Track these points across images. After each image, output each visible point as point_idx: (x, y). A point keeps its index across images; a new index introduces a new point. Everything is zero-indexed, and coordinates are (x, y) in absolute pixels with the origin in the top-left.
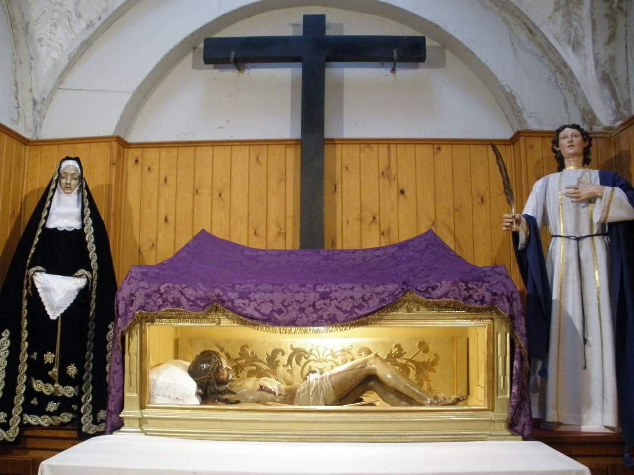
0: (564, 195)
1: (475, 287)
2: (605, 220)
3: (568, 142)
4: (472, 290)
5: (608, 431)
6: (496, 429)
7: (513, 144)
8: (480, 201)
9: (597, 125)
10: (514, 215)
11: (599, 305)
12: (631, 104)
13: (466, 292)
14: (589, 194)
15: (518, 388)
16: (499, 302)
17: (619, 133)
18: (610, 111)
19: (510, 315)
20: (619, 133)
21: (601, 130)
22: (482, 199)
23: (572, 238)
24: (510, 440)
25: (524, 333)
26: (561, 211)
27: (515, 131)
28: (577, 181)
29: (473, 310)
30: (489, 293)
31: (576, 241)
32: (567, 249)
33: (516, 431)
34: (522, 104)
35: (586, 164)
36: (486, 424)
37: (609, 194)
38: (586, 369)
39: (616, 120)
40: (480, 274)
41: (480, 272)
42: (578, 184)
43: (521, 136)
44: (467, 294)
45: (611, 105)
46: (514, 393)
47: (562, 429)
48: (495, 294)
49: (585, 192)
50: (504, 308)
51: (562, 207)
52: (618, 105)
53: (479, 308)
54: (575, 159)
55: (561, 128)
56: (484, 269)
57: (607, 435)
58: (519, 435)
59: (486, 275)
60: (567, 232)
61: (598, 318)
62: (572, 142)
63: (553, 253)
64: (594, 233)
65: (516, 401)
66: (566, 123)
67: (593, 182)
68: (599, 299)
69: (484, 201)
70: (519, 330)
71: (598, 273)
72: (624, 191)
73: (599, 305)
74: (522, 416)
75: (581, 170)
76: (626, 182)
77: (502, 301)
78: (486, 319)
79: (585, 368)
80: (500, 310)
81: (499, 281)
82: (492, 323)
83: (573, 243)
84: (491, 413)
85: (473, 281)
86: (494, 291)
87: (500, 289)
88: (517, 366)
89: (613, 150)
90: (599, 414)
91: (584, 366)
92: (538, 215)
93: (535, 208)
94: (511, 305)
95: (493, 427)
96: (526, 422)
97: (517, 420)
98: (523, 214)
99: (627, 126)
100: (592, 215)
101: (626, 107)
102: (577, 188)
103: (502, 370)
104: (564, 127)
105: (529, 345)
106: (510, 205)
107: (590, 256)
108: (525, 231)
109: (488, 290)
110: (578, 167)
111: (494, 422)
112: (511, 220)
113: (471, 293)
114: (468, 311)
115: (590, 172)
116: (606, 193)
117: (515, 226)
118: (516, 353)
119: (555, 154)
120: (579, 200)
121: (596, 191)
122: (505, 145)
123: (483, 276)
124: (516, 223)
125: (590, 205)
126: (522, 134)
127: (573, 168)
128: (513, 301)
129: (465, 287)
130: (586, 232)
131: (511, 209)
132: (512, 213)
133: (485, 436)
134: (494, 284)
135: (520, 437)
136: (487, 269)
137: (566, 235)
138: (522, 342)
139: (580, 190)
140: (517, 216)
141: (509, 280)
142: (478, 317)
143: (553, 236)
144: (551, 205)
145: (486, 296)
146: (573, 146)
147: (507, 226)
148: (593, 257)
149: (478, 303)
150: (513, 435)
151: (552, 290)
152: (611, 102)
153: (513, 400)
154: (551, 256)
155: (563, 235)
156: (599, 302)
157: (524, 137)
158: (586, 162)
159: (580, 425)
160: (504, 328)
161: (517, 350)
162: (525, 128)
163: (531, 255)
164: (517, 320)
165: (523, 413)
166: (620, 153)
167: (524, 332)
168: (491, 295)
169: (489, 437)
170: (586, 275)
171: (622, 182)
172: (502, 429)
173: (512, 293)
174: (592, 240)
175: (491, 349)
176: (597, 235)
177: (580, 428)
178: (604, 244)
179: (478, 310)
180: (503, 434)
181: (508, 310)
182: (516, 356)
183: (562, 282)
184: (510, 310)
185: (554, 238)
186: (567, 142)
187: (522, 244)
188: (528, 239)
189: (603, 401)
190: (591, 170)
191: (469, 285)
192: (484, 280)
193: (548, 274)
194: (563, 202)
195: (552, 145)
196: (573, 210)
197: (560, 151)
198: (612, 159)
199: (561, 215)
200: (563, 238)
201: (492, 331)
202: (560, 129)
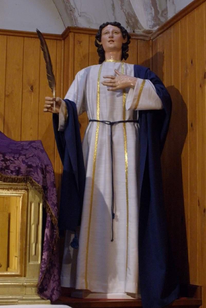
0: (102, 83)
1: (12, 159)
2: (135, 108)
3: (109, 37)
4: (9, 162)
5: (130, 298)
6: (27, 294)
7: (64, 39)
8: (30, 89)
9: (139, 28)
10: (54, 97)
11: (127, 184)
12: (167, 13)
13: (3, 163)
14: (123, 84)
15: (48, 254)
16: (33, 173)
17: (156, 37)
18: (150, 17)
19: (42, 186)
20: (156, 37)
21: (142, 33)
22: (32, 88)
23: (106, 122)
24: (39, 303)
25: (55, 203)
26: (98, 98)
27: (66, 27)
28: (114, 72)
29: (8, 180)
30: (24, 165)
31: (110, 126)
32: (102, 131)
33: (46, 296)
34: (75, 4)
35: (124, 59)
36: (18, 289)
37: (140, 85)
38: (113, 241)
39: (154, 26)
40: (18, 147)
41: (18, 145)
42: (115, 75)
43: (70, 32)
44: (5, 165)
45: (151, 12)
46: (44, 259)
47: (90, 296)
48: (30, 166)
49: (120, 83)
50: (38, 179)
51: (99, 95)
52: (157, 12)
53: (15, 178)
54: (115, 53)
55: (104, 24)
56: (22, 143)
57: (132, 301)
58: (48, 299)
59: (23, 149)
60: (102, 118)
61: (126, 195)
62: (112, 37)
63: (89, 136)
64: (127, 119)
65: (46, 267)
66: (109, 22)
67: (128, 74)
68: (127, 178)
69: (34, 89)
70: (51, 200)
71: (127, 156)
72: (154, 84)
73: (127, 184)
74: (51, 282)
75: (119, 64)
76: (156, 76)
77: (36, 173)
78: (22, 189)
79: (112, 240)
80: (34, 181)
81: (34, 155)
82: (26, 193)
83: (107, 127)
84: (23, 278)
85: (10, 153)
86: (29, 163)
87: (35, 162)
88: (48, 234)
89: (151, 52)
90: (123, 283)
91: (111, 239)
92: (78, 101)
93: (76, 94)
94: (45, 177)
95: (24, 292)
96: (55, 287)
97: (47, 285)
98: (65, 98)
99: (162, 30)
100: (125, 105)
101: (164, 15)
102: (113, 77)
103: (34, 238)
104: (108, 24)
105: (60, 214)
106: (52, 89)
107: (122, 140)
108: (64, 112)
109: (23, 162)
110: (116, 60)
111: (26, 286)
112: (52, 102)
113: (8, 164)
114: (4, 181)
115: (126, 66)
116: (138, 84)
117: (54, 108)
118: (48, 222)
119: (97, 48)
120: (114, 88)
121: (130, 81)
122: (57, 40)
123: (20, 149)
124: (56, 105)
125: (125, 94)
126: (71, 30)
127: (112, 61)
128: (47, 173)
129: (2, 158)
130: (119, 118)
131: (52, 92)
132: (52, 96)
133: (17, 300)
134: (29, 157)
135: (49, 301)
136: (24, 143)
137: (101, 120)
138: (53, 211)
139: (116, 80)
140: (57, 99)
141: (44, 153)
142: (13, 187)
143: (90, 121)
144: (91, 93)
145: (22, 168)
146: (113, 41)
147: (48, 108)
148: (124, 141)
149: (14, 174)
150: (43, 299)
151: (86, 169)
152: (151, 9)
153: (43, 266)
154: (87, 138)
155: (99, 120)
156: (127, 181)
157: (73, 33)
158: (124, 57)
159: (106, 293)
160: (38, 199)
161: (49, 219)
162: (76, 26)
163: (68, 136)
164: (50, 190)
165: (52, 278)
166: (156, 54)
167: (55, 202)
168: (26, 167)
169: (20, 301)
170: (117, 156)
171: (152, 77)
172: (32, 293)
173: (46, 166)
174: (124, 125)
175: (25, 218)
176: (128, 121)
177: (106, 296)
178: (134, 129)
179: (13, 180)
180: (33, 298)
181: (41, 181)
182: (48, 224)
183: (95, 162)
184: (43, 182)
185: (91, 122)
186: (108, 37)
187: (61, 126)
188: (67, 121)
189: (127, 270)
190: (128, 64)
191: (7, 157)
192: (21, 153)
193: (84, 154)
194: (101, 90)
195: (96, 40)
196: (109, 98)
197: (102, 45)
198: (149, 60)
199: (98, 102)
200: (99, 123)
201: (26, 201)
202: (103, 26)
